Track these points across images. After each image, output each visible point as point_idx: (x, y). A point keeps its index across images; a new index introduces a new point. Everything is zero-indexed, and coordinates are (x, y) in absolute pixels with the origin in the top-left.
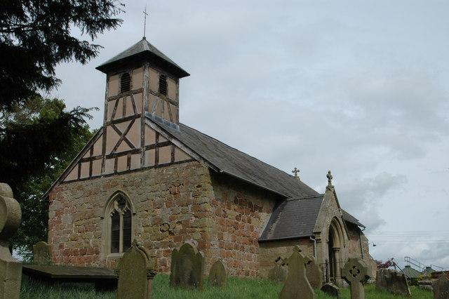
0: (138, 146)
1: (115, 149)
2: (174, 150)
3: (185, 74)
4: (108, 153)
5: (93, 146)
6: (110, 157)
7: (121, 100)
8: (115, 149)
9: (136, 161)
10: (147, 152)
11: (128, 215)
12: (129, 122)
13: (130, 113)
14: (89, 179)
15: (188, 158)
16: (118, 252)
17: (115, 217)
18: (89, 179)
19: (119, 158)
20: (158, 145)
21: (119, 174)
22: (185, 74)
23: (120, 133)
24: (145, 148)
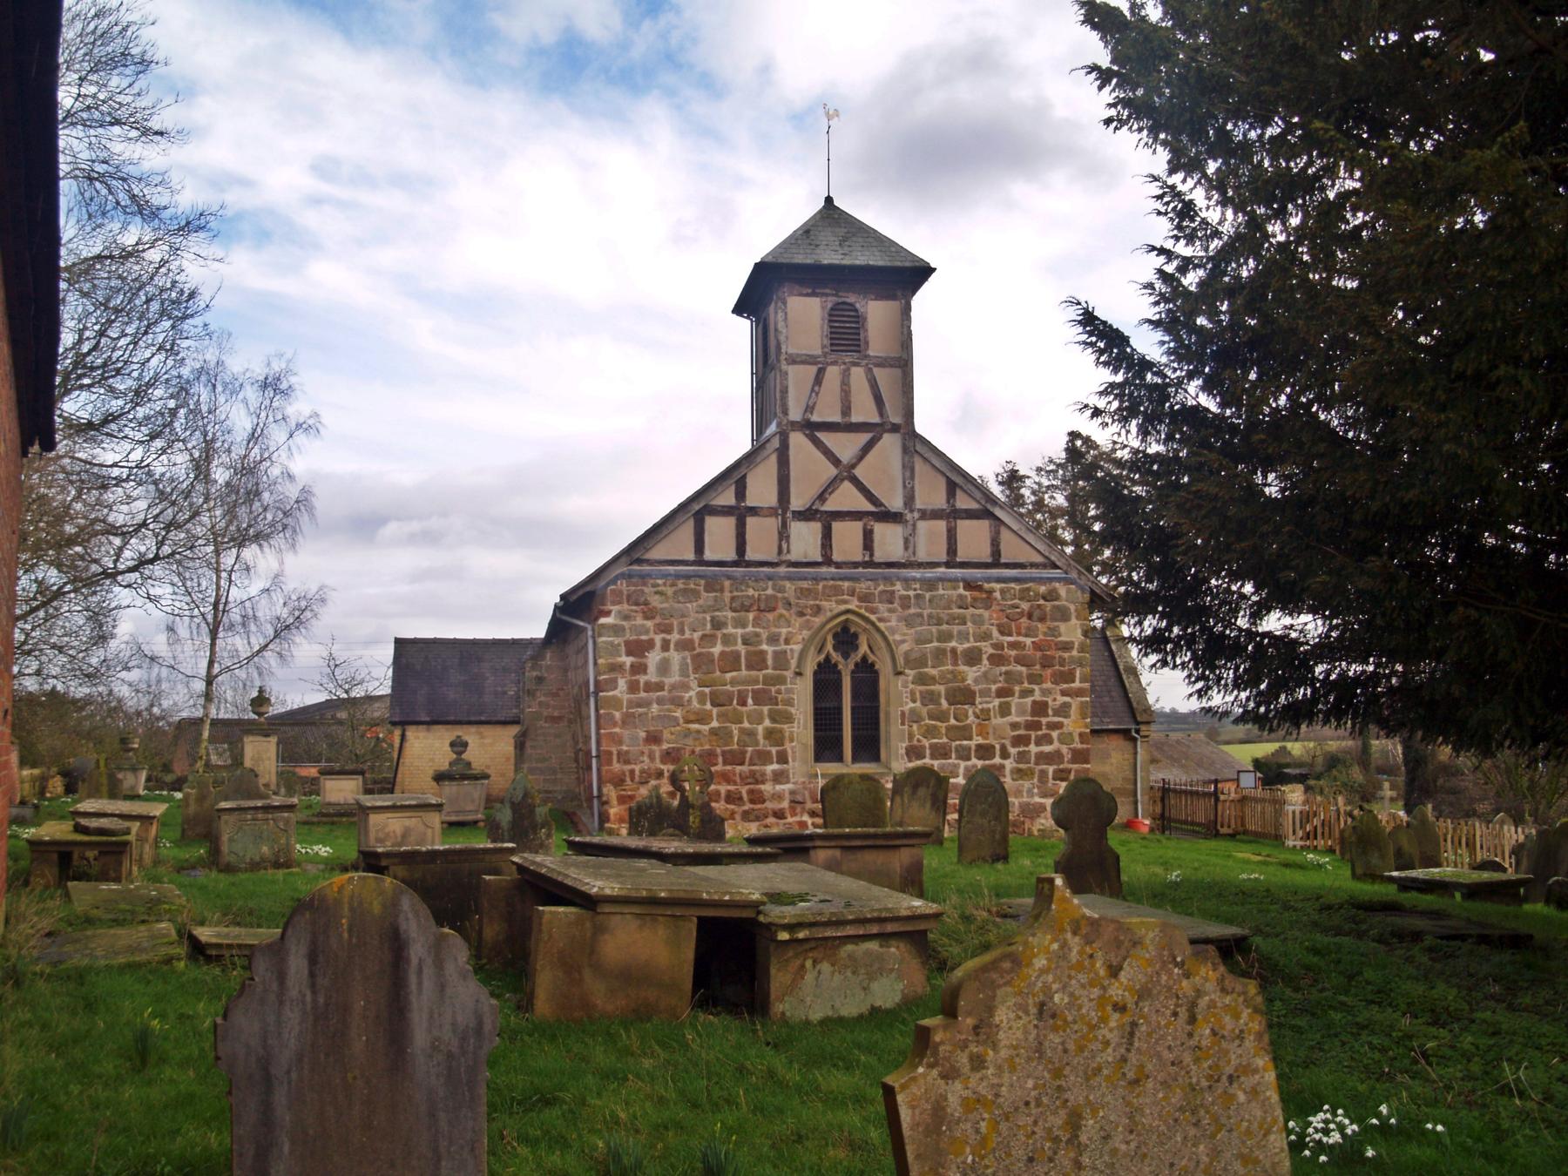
0: (896, 503)
1: (822, 497)
2: (998, 533)
3: (922, 272)
4: (797, 503)
5: (744, 477)
6: (807, 515)
7: (833, 373)
8: (822, 497)
9: (889, 541)
10: (923, 526)
11: (867, 677)
12: (864, 438)
13: (864, 411)
14: (735, 564)
15: (1040, 559)
16: (840, 759)
17: (826, 681)
18: (735, 564)
19: (837, 526)
20: (953, 515)
21: (749, 564)
22: (922, 272)
23: (836, 462)
24: (916, 515)
